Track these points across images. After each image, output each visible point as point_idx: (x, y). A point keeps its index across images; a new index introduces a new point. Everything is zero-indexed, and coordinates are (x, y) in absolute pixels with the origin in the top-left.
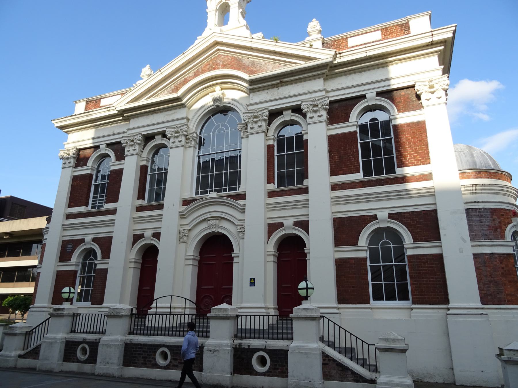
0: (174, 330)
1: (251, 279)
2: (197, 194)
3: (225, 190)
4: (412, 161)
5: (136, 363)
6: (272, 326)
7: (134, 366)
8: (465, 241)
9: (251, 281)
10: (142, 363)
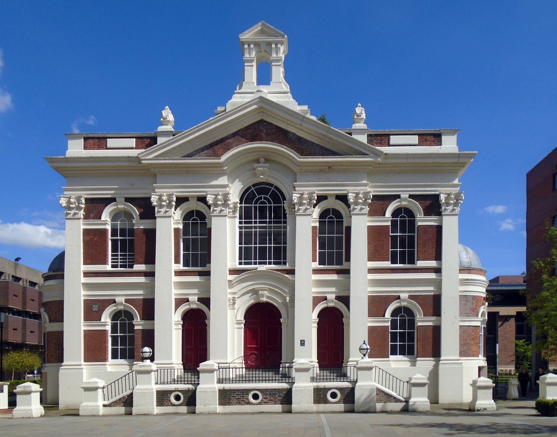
0: (331, 378)
1: (301, 341)
2: (240, 263)
3: (270, 263)
4: (429, 256)
5: (231, 403)
6: (242, 376)
7: (230, 405)
8: (456, 317)
9: (302, 342)
10: (237, 403)
